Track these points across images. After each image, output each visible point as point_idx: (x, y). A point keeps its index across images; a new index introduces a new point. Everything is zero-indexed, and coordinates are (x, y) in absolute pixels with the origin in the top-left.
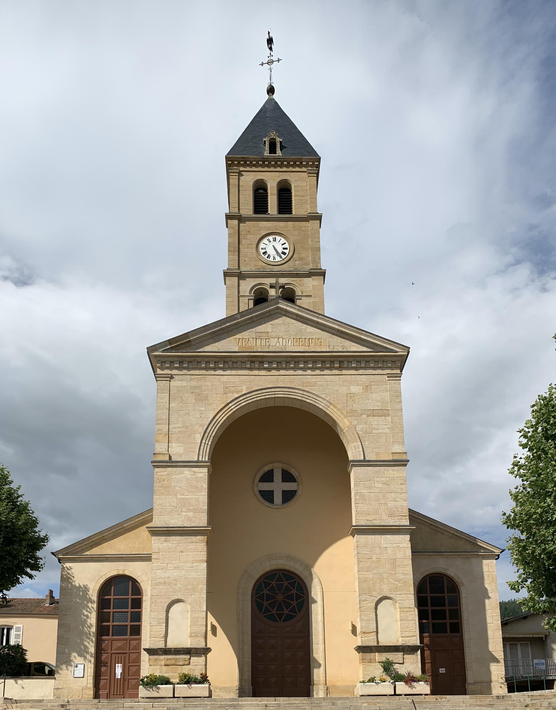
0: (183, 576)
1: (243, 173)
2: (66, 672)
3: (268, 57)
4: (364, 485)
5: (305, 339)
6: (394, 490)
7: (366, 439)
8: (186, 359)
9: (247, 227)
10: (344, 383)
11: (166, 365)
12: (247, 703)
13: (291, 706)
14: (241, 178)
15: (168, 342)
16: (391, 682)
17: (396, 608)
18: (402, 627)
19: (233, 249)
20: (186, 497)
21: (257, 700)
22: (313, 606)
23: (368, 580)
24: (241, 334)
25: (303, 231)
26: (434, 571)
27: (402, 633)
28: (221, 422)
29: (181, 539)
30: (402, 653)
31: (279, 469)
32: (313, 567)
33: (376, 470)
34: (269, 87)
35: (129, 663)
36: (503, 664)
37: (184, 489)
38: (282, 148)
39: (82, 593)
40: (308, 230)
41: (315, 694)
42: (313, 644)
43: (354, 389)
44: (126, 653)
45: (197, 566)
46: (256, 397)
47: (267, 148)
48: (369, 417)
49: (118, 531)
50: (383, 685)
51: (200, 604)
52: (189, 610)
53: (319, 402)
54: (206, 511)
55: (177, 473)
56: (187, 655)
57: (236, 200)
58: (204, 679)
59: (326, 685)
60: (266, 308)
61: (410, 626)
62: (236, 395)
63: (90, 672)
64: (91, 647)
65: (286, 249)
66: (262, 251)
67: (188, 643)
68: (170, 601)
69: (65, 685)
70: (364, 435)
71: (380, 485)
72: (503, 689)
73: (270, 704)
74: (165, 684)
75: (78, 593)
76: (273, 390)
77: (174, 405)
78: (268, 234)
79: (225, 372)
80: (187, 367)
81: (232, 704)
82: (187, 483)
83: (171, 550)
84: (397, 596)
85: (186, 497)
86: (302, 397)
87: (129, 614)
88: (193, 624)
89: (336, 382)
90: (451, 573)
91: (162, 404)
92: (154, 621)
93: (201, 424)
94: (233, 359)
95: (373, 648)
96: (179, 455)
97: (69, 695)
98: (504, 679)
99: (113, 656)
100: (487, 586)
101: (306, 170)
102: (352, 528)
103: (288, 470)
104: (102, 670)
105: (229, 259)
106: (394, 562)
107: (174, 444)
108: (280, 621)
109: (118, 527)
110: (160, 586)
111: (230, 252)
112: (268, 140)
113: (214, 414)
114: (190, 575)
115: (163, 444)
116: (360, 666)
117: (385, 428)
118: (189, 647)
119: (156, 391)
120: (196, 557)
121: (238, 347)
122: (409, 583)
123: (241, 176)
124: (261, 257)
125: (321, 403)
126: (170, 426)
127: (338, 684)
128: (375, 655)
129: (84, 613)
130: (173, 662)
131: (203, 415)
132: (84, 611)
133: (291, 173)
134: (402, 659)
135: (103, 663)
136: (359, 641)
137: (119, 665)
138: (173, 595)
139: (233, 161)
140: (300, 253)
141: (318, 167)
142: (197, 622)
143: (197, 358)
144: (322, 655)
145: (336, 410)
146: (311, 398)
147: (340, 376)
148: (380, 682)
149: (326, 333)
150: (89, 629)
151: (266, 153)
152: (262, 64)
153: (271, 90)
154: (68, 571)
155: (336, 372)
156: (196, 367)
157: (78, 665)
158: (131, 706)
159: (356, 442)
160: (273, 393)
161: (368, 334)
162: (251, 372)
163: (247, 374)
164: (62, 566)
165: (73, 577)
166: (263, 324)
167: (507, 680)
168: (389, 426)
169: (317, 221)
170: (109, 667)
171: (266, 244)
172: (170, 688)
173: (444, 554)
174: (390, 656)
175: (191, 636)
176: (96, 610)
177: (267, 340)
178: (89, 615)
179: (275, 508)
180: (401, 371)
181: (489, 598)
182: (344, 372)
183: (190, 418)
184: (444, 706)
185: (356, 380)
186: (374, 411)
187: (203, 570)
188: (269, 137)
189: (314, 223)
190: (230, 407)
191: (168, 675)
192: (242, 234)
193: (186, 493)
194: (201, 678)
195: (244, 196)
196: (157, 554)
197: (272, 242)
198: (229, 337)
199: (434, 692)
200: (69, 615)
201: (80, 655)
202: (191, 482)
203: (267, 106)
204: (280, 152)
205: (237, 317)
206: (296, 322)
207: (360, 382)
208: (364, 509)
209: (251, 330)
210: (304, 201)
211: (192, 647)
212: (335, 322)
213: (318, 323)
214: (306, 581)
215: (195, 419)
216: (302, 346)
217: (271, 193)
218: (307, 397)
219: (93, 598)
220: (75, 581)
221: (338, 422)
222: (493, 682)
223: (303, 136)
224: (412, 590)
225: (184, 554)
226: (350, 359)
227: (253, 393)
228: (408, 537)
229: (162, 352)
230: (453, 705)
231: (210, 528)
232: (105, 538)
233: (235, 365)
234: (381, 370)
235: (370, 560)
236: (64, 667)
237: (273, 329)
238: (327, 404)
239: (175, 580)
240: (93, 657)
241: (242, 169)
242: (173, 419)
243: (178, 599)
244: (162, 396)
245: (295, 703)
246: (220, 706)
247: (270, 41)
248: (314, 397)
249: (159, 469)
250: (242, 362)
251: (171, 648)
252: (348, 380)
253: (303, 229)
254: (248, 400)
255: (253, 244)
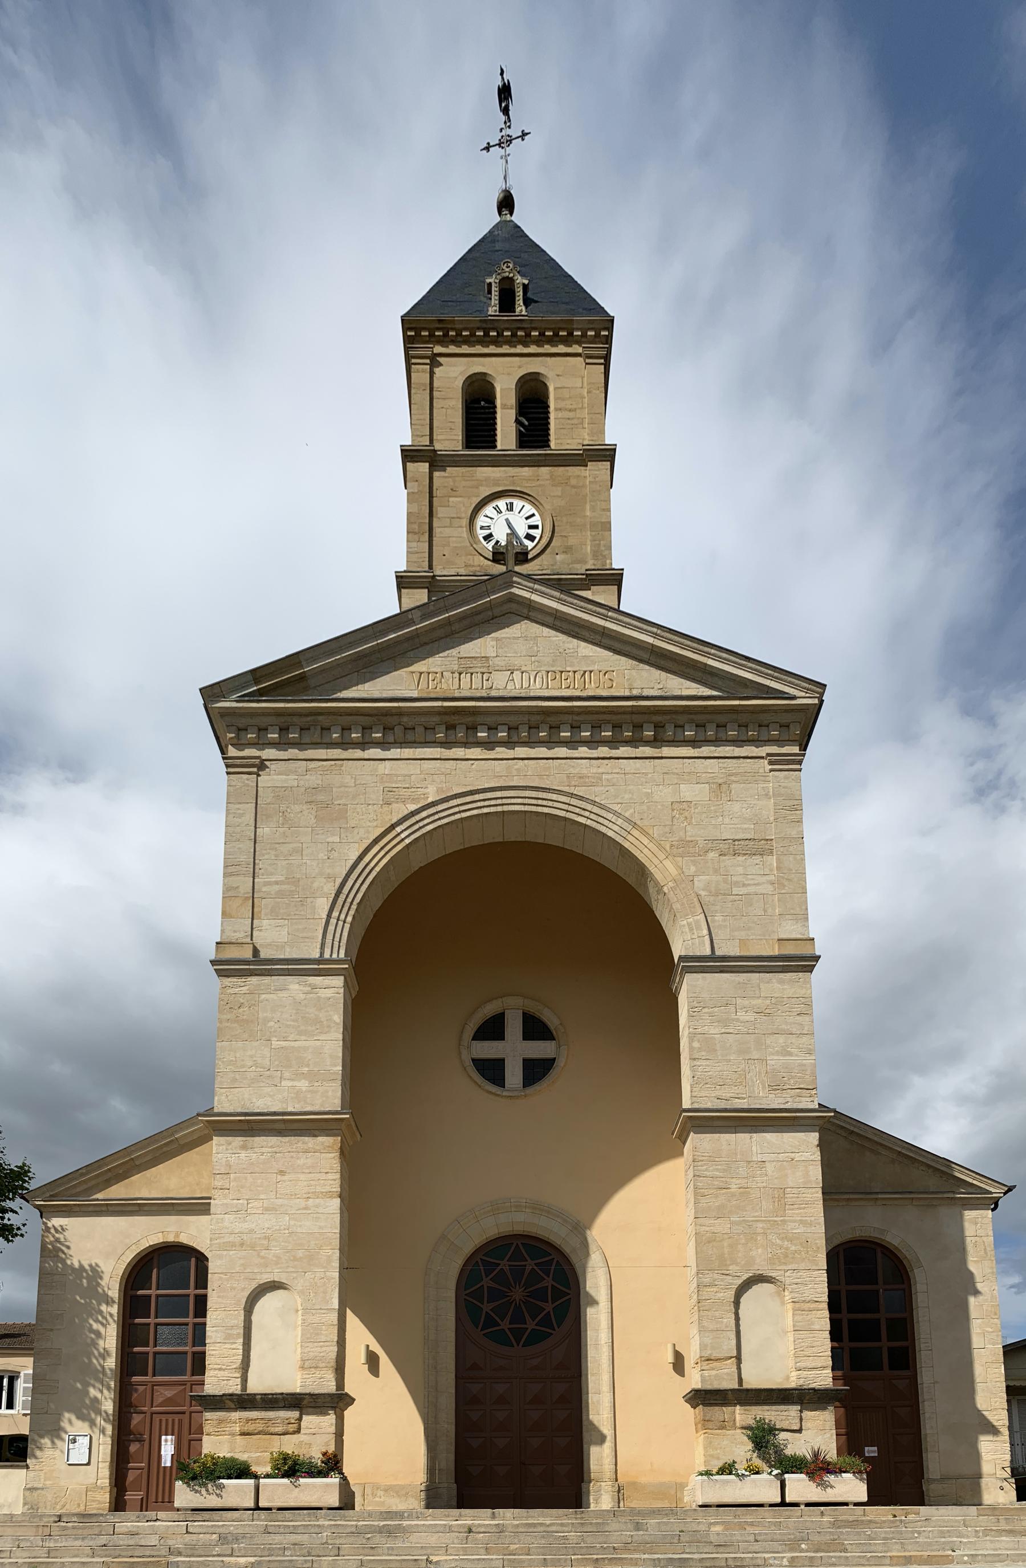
0: (285, 1229)
1: (441, 360)
2: (52, 1453)
3: (501, 130)
4: (711, 1015)
5: (575, 672)
6: (784, 1026)
7: (718, 908)
8: (295, 719)
9: (450, 479)
10: (666, 776)
11: (249, 736)
12: (422, 1523)
13: (531, 1530)
14: (436, 370)
15: (250, 677)
16: (773, 1473)
17: (783, 1303)
18: (798, 1346)
19: (417, 527)
20: (293, 1044)
21: (448, 1516)
22: (590, 1312)
23: (718, 1239)
24: (424, 662)
25: (573, 487)
26: (858, 1234)
27: (798, 1360)
28: (378, 869)
29: (281, 1142)
30: (799, 1408)
31: (517, 1011)
32: (589, 1226)
33: (742, 981)
34: (502, 195)
35: (190, 1434)
36: (1007, 1438)
37: (288, 1026)
38: (527, 302)
39: (88, 1283)
40: (584, 486)
41: (591, 1501)
42: (588, 1394)
43: (688, 791)
44: (184, 1413)
45: (317, 1206)
46: (460, 812)
47: (495, 300)
48: (724, 858)
49: (165, 1149)
50: (754, 1481)
51: (325, 1292)
52: (300, 1308)
53: (606, 822)
54: (340, 1077)
55: (272, 988)
56: (292, 1411)
57: (424, 420)
58: (332, 1464)
59: (617, 1480)
60: (481, 596)
61: (815, 1344)
62: (413, 807)
63: (104, 1454)
64: (106, 1398)
65: (536, 527)
66: (481, 534)
67: (295, 1383)
68: (254, 1285)
69: (50, 1480)
70: (712, 898)
71: (750, 1017)
72: (1006, 1492)
73: (479, 1525)
74: (237, 1477)
75: (78, 1282)
76: (498, 794)
77: (267, 830)
78: (497, 495)
79: (387, 752)
80: (298, 741)
81: (384, 1525)
82: (294, 1011)
83: (257, 1169)
84: (787, 1274)
85: (293, 1044)
86: (567, 811)
87: (190, 1328)
88: (308, 1339)
89: (646, 774)
90: (893, 1238)
91: (238, 829)
92: (216, 1331)
93: (329, 874)
94: (405, 719)
95: (730, 1395)
96: (277, 946)
97: (56, 1503)
98: (1009, 1470)
99: (156, 1418)
100: (972, 1267)
101: (580, 350)
102: (684, 1114)
103: (537, 1014)
104: (130, 1448)
105: (410, 550)
106: (780, 1197)
107: (265, 922)
108: (518, 1345)
109: (163, 1139)
110: (231, 1253)
111: (410, 535)
112: (497, 281)
113: (361, 851)
114: (300, 1226)
115: (239, 920)
116: (697, 1438)
117: (764, 883)
118: (298, 1391)
119: (226, 799)
120: (316, 1185)
121: (416, 691)
122: (816, 1244)
123: (438, 367)
124: (481, 546)
125: (610, 825)
126: (256, 880)
127: (643, 1480)
128: (734, 1412)
129: (91, 1325)
130: (259, 1426)
131: (335, 854)
132: (91, 1322)
133: (548, 359)
134: (798, 1421)
135: (134, 1435)
136: (695, 1379)
137: (169, 1437)
138: (261, 1273)
139: (418, 330)
140: (565, 536)
141: (609, 339)
142: (317, 1334)
143: (320, 718)
144: (607, 1418)
145: (646, 841)
146: (587, 814)
147: (657, 761)
148: (747, 1473)
149: (623, 659)
150: (102, 1362)
151: (493, 309)
152: (487, 148)
153: (506, 203)
154: (57, 1235)
155: (647, 751)
156: (319, 741)
157: (77, 1438)
158: (134, 1530)
159: (694, 914)
160: (499, 802)
161: (724, 655)
162: (448, 751)
163: (438, 757)
164: (45, 1224)
165: (68, 1247)
166: (476, 639)
167: (1014, 1472)
168: (772, 878)
169: (604, 463)
170: (147, 1442)
171: (491, 518)
172: (248, 1486)
173: (880, 1196)
174: (769, 1413)
175: (302, 1368)
176: (116, 1319)
177: (485, 676)
178: (102, 1330)
179: (505, 1096)
180: (804, 747)
181: (976, 1292)
182: (666, 751)
183: (304, 861)
184: (919, 1533)
185: (693, 770)
186: (737, 843)
187: (332, 1216)
188: (499, 274)
189: (597, 469)
190: (399, 834)
191: (248, 1457)
192: (438, 495)
193: (293, 1035)
194: (323, 1462)
195: (444, 410)
196: (225, 1176)
197: (504, 513)
198: (395, 670)
199: (875, 1498)
200: (59, 1329)
201: (81, 1417)
202: (304, 1008)
203: (496, 233)
204: (524, 308)
205: (412, 619)
206: (553, 633)
207: (704, 775)
208: (709, 1073)
209: (447, 652)
210: (575, 421)
211: (304, 1392)
212: (645, 627)
213: (605, 632)
214: (574, 1259)
215: (315, 863)
216: (566, 690)
217: (502, 404)
218: (577, 810)
219: (110, 1293)
220: (71, 1256)
221: (652, 869)
222: (985, 1476)
223: (576, 282)
224: (822, 1261)
225: (285, 1178)
226: (681, 719)
227: (451, 802)
228: (814, 1137)
229: (237, 701)
230: (942, 1532)
231: (348, 1116)
232: (137, 1163)
233: (410, 736)
234: (753, 748)
235: (725, 1190)
236: (46, 1441)
237: (500, 651)
238: (625, 825)
239: (265, 1238)
240: (109, 1419)
241: (438, 349)
242: (263, 864)
243: (274, 1281)
244: (239, 809)
245: (541, 1524)
246: (353, 1530)
247: (505, 92)
248: (596, 810)
249: (230, 979)
250: (426, 728)
251: (255, 1395)
252: (675, 771)
253: (573, 482)
254: (440, 819)
255: (463, 518)
